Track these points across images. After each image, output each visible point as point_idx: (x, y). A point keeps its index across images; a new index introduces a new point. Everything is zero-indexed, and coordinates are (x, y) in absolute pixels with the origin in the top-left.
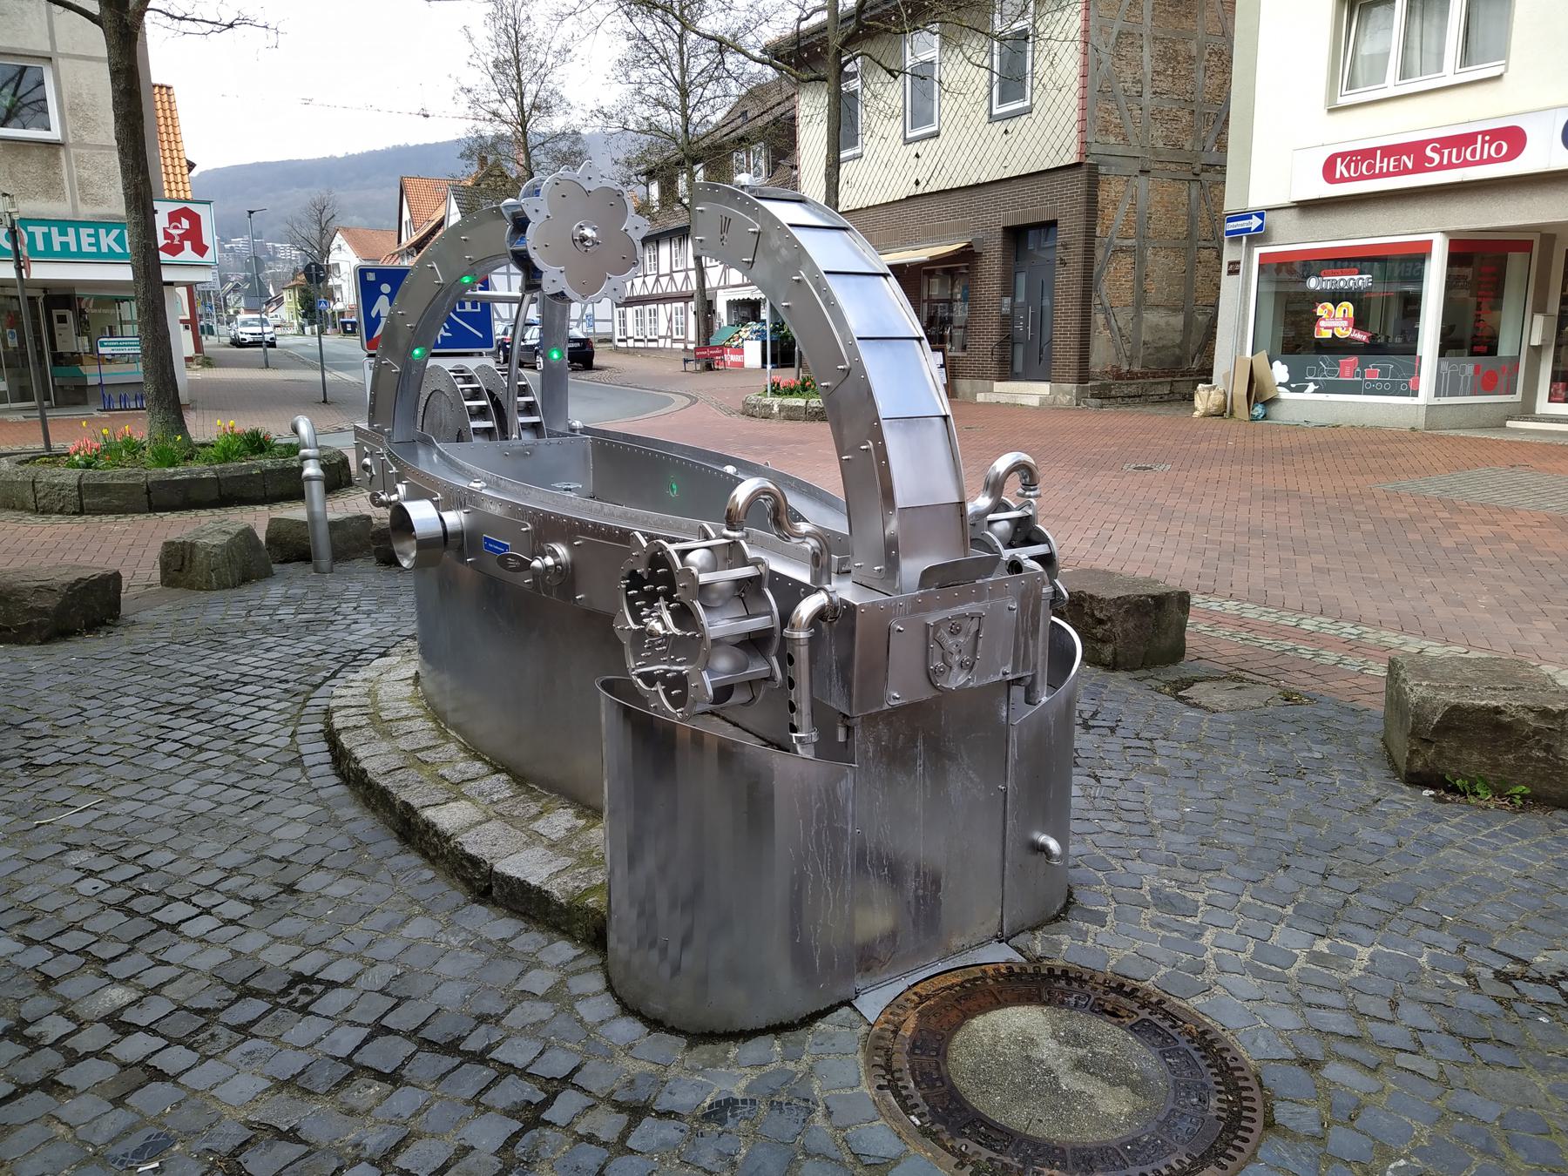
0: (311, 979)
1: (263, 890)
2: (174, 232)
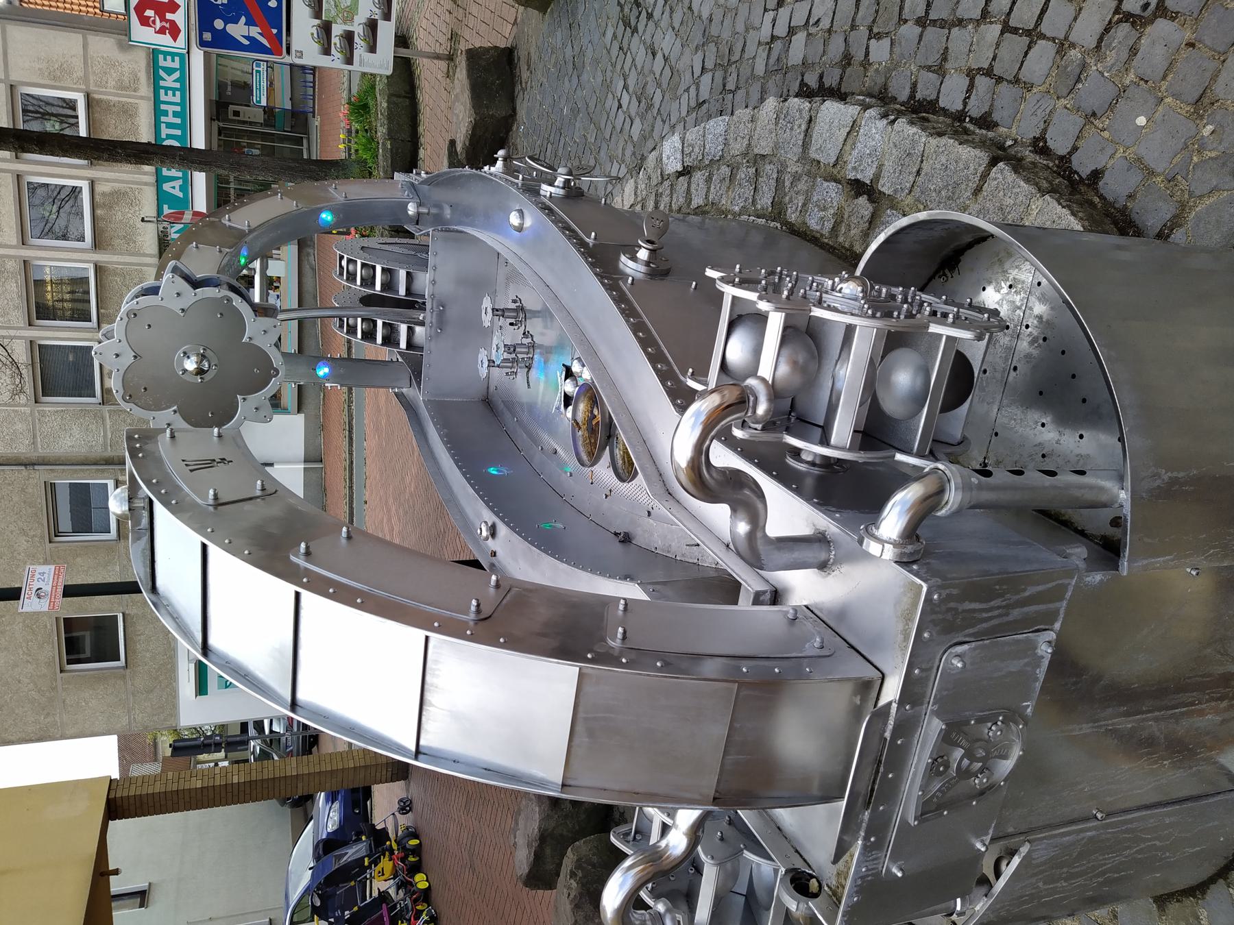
2: (158, 25)
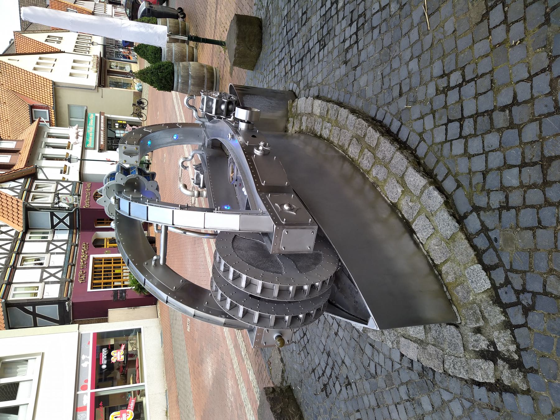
0: (323, 48)
1: (349, 56)
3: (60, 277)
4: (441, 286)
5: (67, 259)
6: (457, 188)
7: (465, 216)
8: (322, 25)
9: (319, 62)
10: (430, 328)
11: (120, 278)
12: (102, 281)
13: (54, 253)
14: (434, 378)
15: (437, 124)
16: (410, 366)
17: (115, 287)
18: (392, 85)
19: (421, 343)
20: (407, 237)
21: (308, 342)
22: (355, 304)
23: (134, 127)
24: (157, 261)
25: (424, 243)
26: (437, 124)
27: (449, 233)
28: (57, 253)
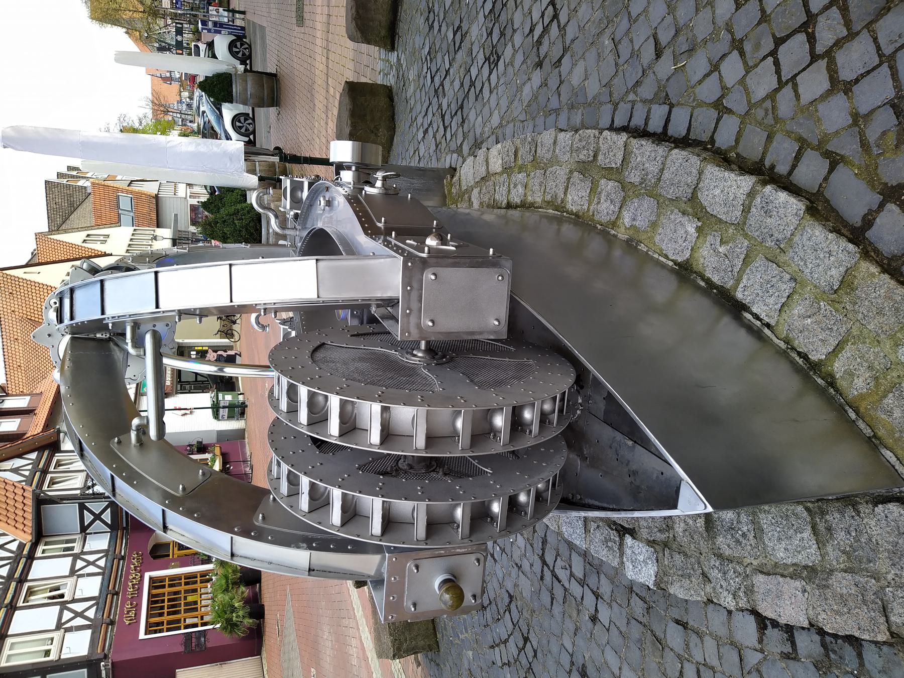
0: (496, 65)
1: (544, 49)
3: (92, 617)
4: (840, 410)
5: (106, 583)
6: (831, 169)
7: (868, 222)
8: (489, 31)
9: (491, 92)
10: (829, 529)
11: (196, 609)
12: (165, 618)
13: (82, 576)
14: (862, 664)
15: (751, 64)
16: (788, 649)
17: (186, 627)
18: (636, 48)
19: (809, 573)
20: (726, 321)
21: (535, 656)
22: (632, 479)
23: (219, 353)
24: (143, 430)
25: (773, 322)
26: (751, 64)
27: (836, 274)
28: (89, 575)
